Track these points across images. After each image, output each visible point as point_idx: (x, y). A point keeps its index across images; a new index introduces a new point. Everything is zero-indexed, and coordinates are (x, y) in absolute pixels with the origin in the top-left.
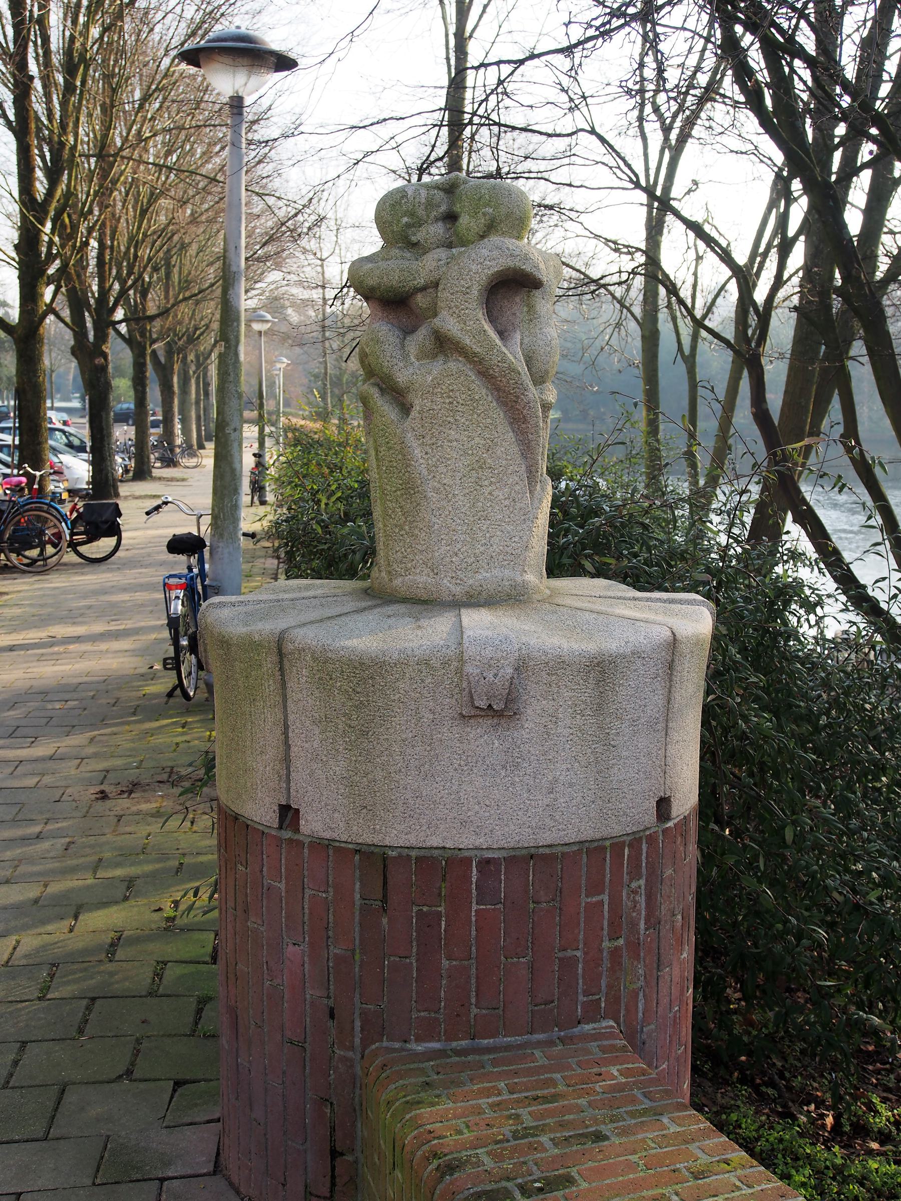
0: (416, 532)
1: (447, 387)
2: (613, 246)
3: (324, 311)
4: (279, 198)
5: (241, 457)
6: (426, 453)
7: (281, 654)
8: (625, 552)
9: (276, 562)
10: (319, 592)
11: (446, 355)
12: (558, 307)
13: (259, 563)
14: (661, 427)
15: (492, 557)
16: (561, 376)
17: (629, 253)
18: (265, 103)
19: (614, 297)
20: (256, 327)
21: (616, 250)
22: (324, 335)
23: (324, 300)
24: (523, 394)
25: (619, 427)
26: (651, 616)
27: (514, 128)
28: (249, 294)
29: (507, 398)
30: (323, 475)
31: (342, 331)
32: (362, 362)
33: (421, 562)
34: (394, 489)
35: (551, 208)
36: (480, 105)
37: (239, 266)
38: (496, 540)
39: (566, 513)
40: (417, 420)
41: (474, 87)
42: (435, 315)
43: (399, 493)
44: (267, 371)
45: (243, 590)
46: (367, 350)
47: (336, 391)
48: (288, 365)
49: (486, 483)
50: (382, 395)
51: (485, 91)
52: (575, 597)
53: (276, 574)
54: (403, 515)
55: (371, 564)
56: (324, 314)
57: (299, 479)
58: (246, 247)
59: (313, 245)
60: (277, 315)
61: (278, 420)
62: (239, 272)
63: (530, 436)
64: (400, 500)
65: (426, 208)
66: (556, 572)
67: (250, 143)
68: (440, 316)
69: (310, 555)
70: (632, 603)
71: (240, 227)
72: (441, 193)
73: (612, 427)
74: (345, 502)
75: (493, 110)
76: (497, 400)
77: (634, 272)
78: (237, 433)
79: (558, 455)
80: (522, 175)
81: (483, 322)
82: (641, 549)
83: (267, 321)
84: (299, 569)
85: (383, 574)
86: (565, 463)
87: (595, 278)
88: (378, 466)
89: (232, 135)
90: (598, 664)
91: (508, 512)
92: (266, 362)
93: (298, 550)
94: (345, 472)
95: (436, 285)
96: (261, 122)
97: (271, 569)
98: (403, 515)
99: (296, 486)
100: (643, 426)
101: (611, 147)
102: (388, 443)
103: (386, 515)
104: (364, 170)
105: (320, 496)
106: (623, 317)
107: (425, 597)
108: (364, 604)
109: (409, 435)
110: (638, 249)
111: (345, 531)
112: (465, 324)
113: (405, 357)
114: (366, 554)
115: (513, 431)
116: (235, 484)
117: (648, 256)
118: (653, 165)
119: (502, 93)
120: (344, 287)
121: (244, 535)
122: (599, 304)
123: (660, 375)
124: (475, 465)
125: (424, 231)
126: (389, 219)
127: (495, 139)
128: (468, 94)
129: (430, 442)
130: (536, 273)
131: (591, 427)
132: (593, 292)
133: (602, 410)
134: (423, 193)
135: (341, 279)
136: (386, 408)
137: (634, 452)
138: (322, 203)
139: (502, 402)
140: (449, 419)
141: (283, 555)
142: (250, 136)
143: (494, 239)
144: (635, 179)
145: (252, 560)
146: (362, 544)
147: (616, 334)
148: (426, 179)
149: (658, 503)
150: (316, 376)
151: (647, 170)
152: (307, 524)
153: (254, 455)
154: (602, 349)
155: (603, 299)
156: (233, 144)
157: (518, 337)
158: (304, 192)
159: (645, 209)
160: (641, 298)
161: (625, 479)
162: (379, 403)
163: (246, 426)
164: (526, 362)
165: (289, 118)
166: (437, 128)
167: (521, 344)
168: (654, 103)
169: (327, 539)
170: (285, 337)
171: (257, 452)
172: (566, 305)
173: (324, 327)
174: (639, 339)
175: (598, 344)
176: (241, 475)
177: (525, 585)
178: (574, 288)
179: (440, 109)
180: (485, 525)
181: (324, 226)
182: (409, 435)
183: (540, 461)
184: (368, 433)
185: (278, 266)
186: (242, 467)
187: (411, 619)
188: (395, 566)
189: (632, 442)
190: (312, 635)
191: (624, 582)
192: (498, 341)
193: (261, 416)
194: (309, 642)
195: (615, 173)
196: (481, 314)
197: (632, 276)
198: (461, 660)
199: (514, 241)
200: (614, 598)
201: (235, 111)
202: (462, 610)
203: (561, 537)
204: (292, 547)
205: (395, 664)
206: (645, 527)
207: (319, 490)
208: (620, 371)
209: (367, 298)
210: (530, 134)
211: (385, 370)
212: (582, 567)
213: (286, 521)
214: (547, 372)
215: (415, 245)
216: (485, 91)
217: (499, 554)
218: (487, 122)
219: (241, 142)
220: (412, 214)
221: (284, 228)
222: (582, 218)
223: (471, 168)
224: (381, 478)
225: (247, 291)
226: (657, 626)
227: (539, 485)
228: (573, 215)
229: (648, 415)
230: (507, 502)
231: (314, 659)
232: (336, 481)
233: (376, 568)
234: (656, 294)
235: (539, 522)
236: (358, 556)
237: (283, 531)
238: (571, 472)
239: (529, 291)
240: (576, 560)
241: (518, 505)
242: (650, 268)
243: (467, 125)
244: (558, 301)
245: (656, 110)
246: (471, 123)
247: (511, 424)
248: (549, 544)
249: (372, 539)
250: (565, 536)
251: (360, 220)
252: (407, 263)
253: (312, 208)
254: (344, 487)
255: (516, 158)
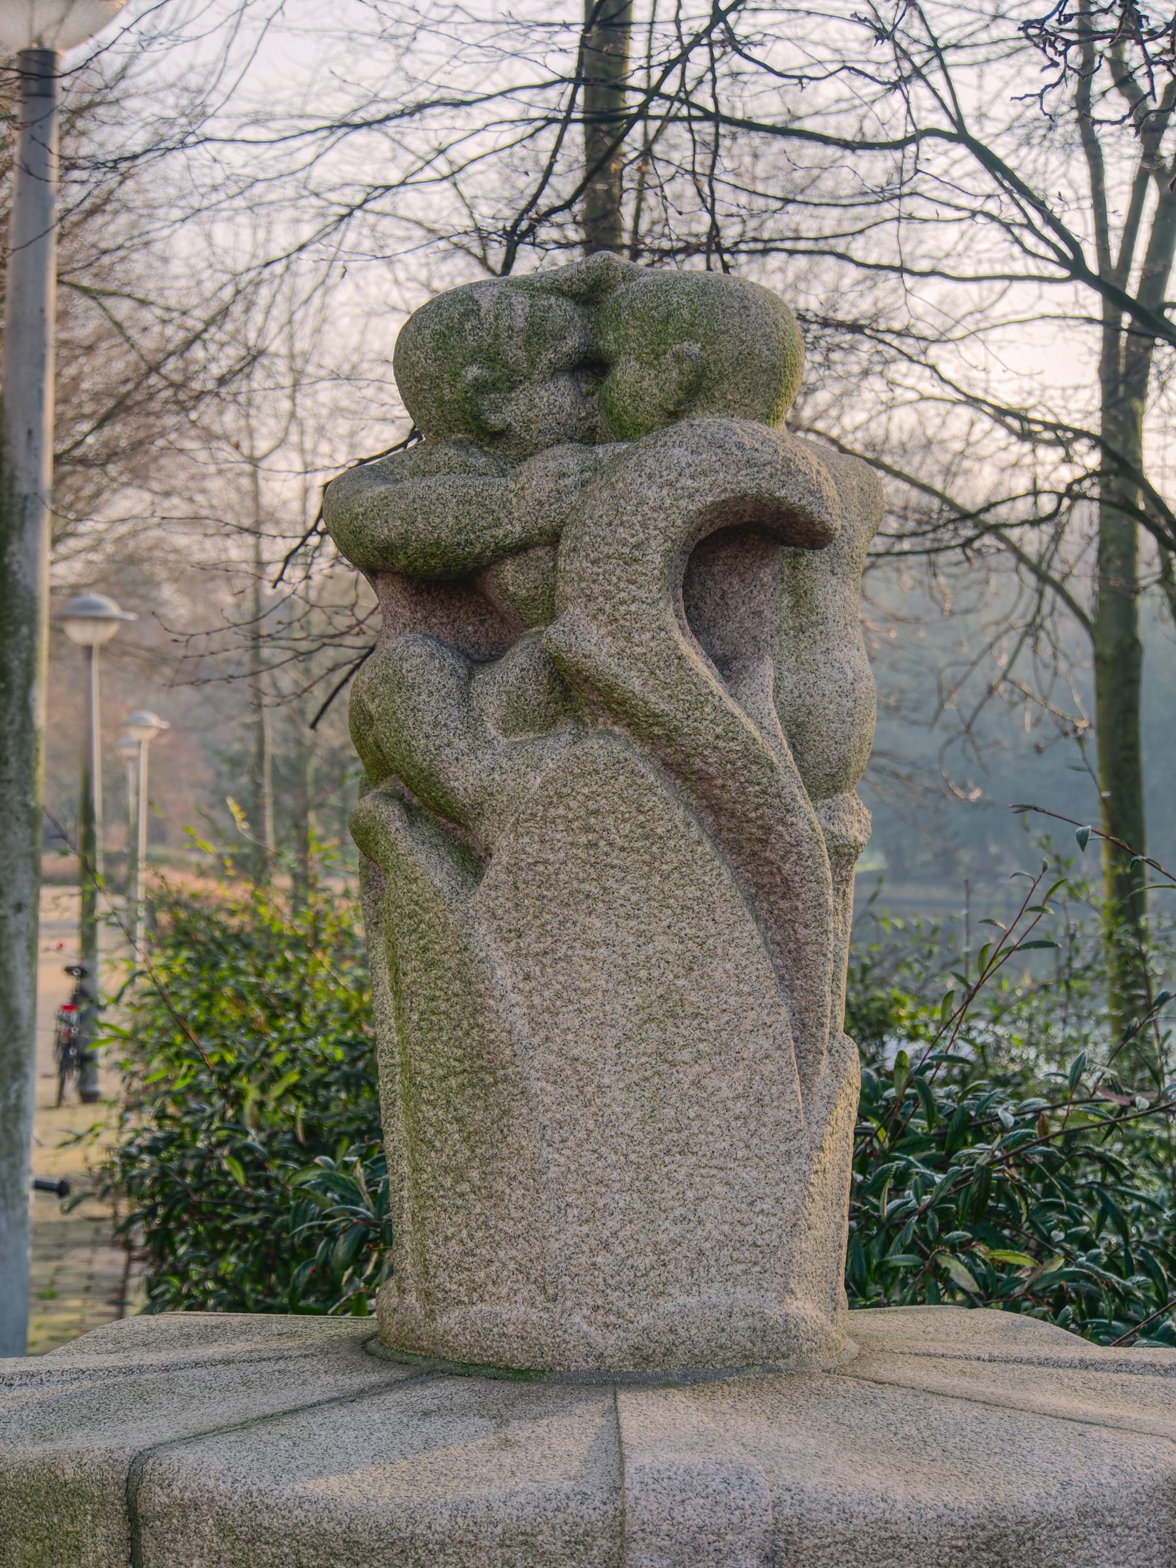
0: (500, 1185)
1: (583, 804)
2: (1016, 424)
3: (257, 591)
4: (143, 303)
5: (34, 977)
6: (527, 977)
7: (134, 1518)
8: (1058, 1235)
9: (121, 1257)
10: (239, 1347)
11: (579, 720)
12: (874, 582)
13: (77, 1261)
14: (1152, 895)
15: (701, 1253)
16: (882, 761)
17: (1058, 442)
18: (112, 62)
19: (1021, 557)
20: (78, 633)
21: (1025, 436)
22: (256, 658)
23: (260, 564)
24: (782, 821)
25: (1036, 900)
26: (1130, 1412)
27: (749, 125)
28: (62, 549)
29: (740, 831)
30: (247, 1023)
31: (304, 646)
32: (359, 738)
33: (512, 1266)
34: (440, 1072)
35: (855, 328)
36: (666, 73)
37: (36, 481)
38: (710, 1208)
39: (898, 1131)
40: (505, 890)
41: (652, 23)
42: (551, 615)
43: (453, 1082)
44: (107, 748)
45: (33, 1335)
46: (372, 707)
47: (288, 800)
48: (162, 733)
49: (686, 1055)
50: (412, 824)
51: (679, 38)
52: (924, 1361)
53: (122, 1291)
54: (465, 1140)
55: (378, 1266)
56: (257, 600)
57: (187, 1037)
58: (56, 427)
59: (230, 419)
60: (134, 602)
61: (131, 879)
62: (35, 497)
63: (802, 932)
64: (457, 1101)
65: (528, 341)
66: (874, 1288)
67: (70, 165)
68: (564, 618)
69: (213, 1241)
70: (1078, 1376)
71: (41, 379)
72: (567, 305)
73: (1018, 898)
74: (309, 1100)
75: (700, 81)
76: (715, 837)
77: (1072, 494)
78: (23, 917)
79: (876, 972)
80: (778, 245)
81: (677, 634)
82: (1100, 1225)
83: (108, 620)
84: (184, 1276)
85: (411, 1299)
86: (896, 993)
87: (971, 507)
88: (399, 1009)
89: (24, 150)
90: (988, 1545)
91: (743, 1133)
92: (104, 725)
93: (182, 1226)
94: (309, 1017)
95: (553, 539)
96: (101, 111)
97: (108, 1278)
98: (465, 1140)
99: (178, 1055)
100: (1100, 892)
101: (1008, 174)
102: (425, 950)
103: (419, 1139)
104: (366, 231)
105: (242, 1082)
106: (1046, 609)
107: (522, 1361)
108: (357, 1381)
109: (482, 930)
110: (1079, 434)
111: (311, 1176)
112: (628, 639)
113: (473, 723)
114: (363, 1239)
115: (757, 919)
116: (17, 1052)
117: (1108, 453)
118: (1117, 221)
119: (722, 43)
120: (309, 534)
121: (39, 1186)
122: (981, 575)
123: (1145, 756)
124: (654, 1009)
125: (523, 402)
126: (433, 369)
127: (704, 158)
128: (637, 47)
129: (536, 948)
130: (814, 508)
131: (962, 896)
132: (968, 542)
133: (994, 849)
134: (521, 304)
135: (304, 511)
136: (421, 858)
137: (1077, 964)
138: (257, 317)
139: (726, 842)
140: (586, 887)
141: (140, 1240)
142: (71, 146)
143: (706, 422)
144: (1070, 255)
145: (57, 1251)
146: (355, 1213)
147: (1026, 651)
148: (527, 262)
149: (1143, 1102)
150: (235, 762)
151: (1102, 230)
152: (207, 1155)
153: (69, 970)
154: (991, 690)
155: (993, 561)
156: (27, 170)
157: (768, 670)
158: (209, 287)
159: (1098, 331)
160: (1092, 555)
161: (1058, 1033)
162: (403, 848)
163: (47, 893)
164: (791, 736)
165: (171, 100)
166: (556, 128)
167: (777, 689)
168: (1117, 64)
169: (258, 1200)
170: (155, 660)
171: (74, 962)
172: (893, 575)
173: (256, 637)
174: (1088, 664)
175: (980, 677)
176: (32, 1028)
177: (789, 1327)
178: (914, 534)
179: (563, 80)
180: (682, 1168)
181: (258, 375)
182: (482, 930)
183: (829, 999)
184: (373, 924)
185: (139, 477)
186: (34, 1006)
187: (485, 1422)
188: (443, 1277)
189: (1072, 937)
190: (216, 1464)
191: (1055, 1315)
192: (716, 686)
193: (88, 869)
194: (211, 1483)
195: (1018, 241)
196: (670, 616)
197: (1066, 502)
198: (620, 1534)
199: (755, 425)
200: (1029, 1362)
201: (34, 86)
202: (622, 1397)
203: (885, 1196)
204: (166, 1219)
205: (442, 1544)
206: (1109, 1165)
207: (239, 1067)
208: (1038, 750)
209: (372, 573)
210: (796, 142)
211: (418, 758)
212: (942, 1275)
213: (152, 1150)
214: (844, 763)
215: (498, 435)
216: (679, 38)
217: (722, 1245)
218: (684, 112)
219: (47, 165)
220: (491, 358)
221: (153, 380)
222: (935, 353)
223: (643, 227)
224: (405, 1041)
225: (56, 541)
226: (1147, 1440)
227: (825, 1059)
228: (909, 346)
229: (1114, 867)
230: (740, 1107)
231: (224, 1531)
232: (287, 1042)
233: (391, 1284)
234: (1129, 551)
235: (827, 1158)
236: (342, 1248)
237: (142, 1176)
238: (912, 1017)
239: (796, 555)
240: (925, 1256)
241: (771, 1115)
242: (1115, 483)
243: (631, 120)
244: (873, 566)
245: (1124, 81)
246: (643, 113)
247: (751, 899)
248: (854, 1213)
249: (381, 1201)
250: (897, 1191)
251: (355, 358)
252: (479, 482)
253: (229, 327)
254: (306, 1057)
255: (760, 203)
